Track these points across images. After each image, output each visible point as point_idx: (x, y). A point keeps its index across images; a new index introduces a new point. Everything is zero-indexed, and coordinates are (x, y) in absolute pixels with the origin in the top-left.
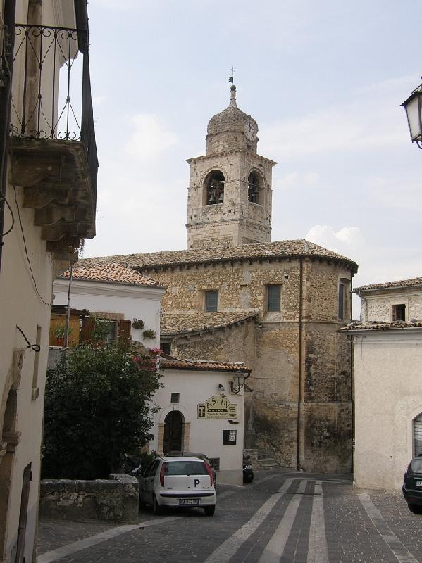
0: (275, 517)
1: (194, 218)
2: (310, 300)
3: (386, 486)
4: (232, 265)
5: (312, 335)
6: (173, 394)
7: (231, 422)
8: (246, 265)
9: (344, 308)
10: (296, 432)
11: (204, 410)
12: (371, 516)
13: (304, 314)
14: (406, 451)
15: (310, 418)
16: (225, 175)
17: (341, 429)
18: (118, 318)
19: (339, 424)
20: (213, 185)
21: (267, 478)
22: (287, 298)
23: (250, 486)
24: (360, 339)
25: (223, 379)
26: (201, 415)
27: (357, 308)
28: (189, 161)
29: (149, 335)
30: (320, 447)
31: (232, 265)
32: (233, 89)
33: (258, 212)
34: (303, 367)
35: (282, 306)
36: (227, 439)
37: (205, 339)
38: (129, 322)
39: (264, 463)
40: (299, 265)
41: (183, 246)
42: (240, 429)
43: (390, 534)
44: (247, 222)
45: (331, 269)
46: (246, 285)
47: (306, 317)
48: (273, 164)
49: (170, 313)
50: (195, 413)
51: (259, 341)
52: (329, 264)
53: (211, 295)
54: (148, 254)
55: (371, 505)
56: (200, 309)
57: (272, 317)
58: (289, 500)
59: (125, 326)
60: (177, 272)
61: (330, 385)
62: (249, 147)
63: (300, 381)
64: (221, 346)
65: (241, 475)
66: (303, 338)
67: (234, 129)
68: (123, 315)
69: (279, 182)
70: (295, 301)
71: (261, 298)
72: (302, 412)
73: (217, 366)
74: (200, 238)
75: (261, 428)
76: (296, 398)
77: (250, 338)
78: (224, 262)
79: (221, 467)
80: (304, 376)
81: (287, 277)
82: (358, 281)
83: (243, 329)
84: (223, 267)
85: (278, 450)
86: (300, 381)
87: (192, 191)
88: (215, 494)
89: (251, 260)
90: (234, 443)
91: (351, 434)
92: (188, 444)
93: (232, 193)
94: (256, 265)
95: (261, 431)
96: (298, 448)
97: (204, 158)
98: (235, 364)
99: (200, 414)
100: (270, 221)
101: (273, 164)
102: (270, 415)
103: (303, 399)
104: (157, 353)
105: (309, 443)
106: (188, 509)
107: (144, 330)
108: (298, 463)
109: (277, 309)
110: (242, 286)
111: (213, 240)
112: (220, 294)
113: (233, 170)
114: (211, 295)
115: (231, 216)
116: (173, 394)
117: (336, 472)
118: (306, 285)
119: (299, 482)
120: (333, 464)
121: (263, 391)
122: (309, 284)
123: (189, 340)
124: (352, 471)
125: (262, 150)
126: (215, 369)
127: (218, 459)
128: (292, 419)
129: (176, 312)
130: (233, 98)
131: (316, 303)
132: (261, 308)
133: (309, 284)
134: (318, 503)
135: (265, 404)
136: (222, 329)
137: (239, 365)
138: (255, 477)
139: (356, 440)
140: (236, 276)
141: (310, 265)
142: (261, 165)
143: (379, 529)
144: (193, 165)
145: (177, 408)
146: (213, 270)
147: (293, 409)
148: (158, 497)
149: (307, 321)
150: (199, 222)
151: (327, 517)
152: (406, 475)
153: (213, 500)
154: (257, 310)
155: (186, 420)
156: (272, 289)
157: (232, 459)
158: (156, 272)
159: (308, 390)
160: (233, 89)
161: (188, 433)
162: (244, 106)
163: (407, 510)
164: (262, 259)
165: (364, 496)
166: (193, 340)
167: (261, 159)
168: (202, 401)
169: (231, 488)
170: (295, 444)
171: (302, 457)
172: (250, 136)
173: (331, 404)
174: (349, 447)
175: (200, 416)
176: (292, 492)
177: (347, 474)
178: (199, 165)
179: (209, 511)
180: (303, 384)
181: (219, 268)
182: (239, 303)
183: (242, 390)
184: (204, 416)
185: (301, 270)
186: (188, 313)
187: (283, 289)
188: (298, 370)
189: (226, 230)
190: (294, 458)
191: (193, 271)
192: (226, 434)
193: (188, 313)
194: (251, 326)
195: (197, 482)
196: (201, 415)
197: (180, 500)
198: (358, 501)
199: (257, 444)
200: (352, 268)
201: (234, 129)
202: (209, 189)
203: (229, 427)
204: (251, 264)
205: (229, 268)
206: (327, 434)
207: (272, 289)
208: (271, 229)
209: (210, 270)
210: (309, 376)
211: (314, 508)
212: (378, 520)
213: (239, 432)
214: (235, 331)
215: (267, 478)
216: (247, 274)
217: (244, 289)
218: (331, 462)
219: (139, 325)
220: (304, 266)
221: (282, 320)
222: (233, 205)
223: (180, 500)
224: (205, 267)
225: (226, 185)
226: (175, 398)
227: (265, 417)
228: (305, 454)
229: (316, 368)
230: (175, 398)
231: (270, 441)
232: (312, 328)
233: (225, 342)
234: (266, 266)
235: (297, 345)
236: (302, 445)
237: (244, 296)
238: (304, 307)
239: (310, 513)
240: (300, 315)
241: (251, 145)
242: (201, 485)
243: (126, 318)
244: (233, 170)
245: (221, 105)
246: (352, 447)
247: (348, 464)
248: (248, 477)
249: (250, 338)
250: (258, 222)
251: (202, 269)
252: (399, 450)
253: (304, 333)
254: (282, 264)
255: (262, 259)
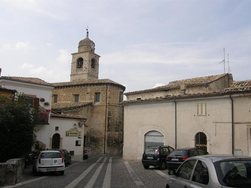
0: (94, 169)
1: (73, 73)
2: (110, 98)
3: (134, 159)
4: (84, 86)
5: (110, 110)
6: (56, 127)
7: (79, 138)
8: (89, 86)
9: (121, 99)
10: (104, 142)
11: (68, 133)
12: (130, 171)
13: (108, 102)
14: (142, 146)
15: (109, 137)
16: (84, 59)
17: (119, 140)
18: (34, 97)
19: (118, 139)
20: (79, 62)
21: (93, 157)
22: (102, 97)
23: (86, 160)
24: (126, 107)
25: (76, 122)
26: (67, 135)
27: (125, 98)
28: (72, 54)
29: (47, 104)
30: (112, 146)
31: (84, 86)
32: (88, 32)
33: (94, 71)
34: (107, 120)
35: (100, 100)
36: (77, 144)
37: (73, 110)
38: (38, 99)
39: (93, 152)
40: (106, 86)
41: (69, 81)
42: (82, 140)
43: (138, 180)
44: (90, 74)
45: (117, 88)
46: (88, 93)
47: (108, 104)
48: (100, 57)
49: (62, 102)
50: (65, 134)
51: (92, 110)
52: (116, 86)
53: (77, 96)
54: (56, 83)
55: (130, 166)
56: (73, 101)
57: (97, 104)
58: (99, 166)
59: (37, 100)
60: (65, 89)
61: (116, 126)
62: (92, 51)
63: (106, 125)
64: (79, 113)
65: (82, 156)
66: (107, 111)
67: (87, 45)
68: (36, 96)
69: (101, 61)
70: (105, 98)
71: (93, 97)
72: (106, 135)
73: (74, 117)
74: (74, 79)
75: (90, 140)
76: (104, 130)
77: (89, 111)
78: (81, 85)
79: (75, 154)
80: (107, 123)
81: (102, 90)
82: (125, 92)
83: (87, 107)
84: (81, 87)
85: (98, 147)
86: (106, 125)
87: (73, 64)
88: (64, 166)
89: (91, 85)
90: (80, 145)
91: (122, 142)
92: (62, 146)
93: (86, 65)
94: (92, 86)
95: (92, 142)
96: (105, 147)
97: (77, 53)
98: (81, 117)
99: (67, 135)
100: (98, 75)
101: (100, 57)
102: (95, 136)
103: (107, 131)
104: (49, 111)
105: (108, 145)
106: (53, 173)
107: (45, 102)
108: (104, 152)
109: (99, 101)
110: (87, 93)
111: (79, 80)
112: (79, 96)
113: (86, 57)
114: (77, 96)
115: (85, 72)
116: (56, 127)
117: (117, 154)
118: (108, 93)
119: (104, 158)
120: (116, 152)
121: (93, 128)
122: (109, 93)
123: (67, 111)
124: (122, 153)
125: (96, 52)
126: (73, 118)
127: (74, 151)
128: (103, 138)
129: (64, 102)
130: (87, 35)
131: (112, 99)
132: (94, 101)
133: (109, 93)
134: (109, 165)
135: (94, 133)
136: (79, 107)
137: (82, 117)
138: (88, 157)
139: (124, 143)
140: (85, 90)
141: (110, 86)
142: (95, 57)
143: (133, 178)
144: (74, 56)
145: (57, 132)
146: (77, 88)
147: (103, 134)
148: (37, 168)
149: (109, 105)
150: (74, 74)
151: (112, 173)
152: (143, 155)
153: (63, 169)
154: (92, 101)
155: (61, 137)
156: (97, 94)
157: (79, 151)
158: (58, 88)
159: (108, 128)
160: (88, 32)
161: (62, 142)
162: (91, 38)
163: (143, 167)
164: (94, 84)
165: (126, 163)
166: (69, 111)
167: (96, 55)
168: (68, 130)
169: (78, 162)
170: (104, 146)
171: (106, 150)
172: (92, 47)
173: (116, 132)
174: (121, 146)
175: (67, 135)
176: (101, 162)
177: (121, 154)
178: (75, 55)
179: (62, 173)
180: (107, 126)
181: (80, 87)
182: (86, 99)
183: (83, 126)
184: (68, 135)
185: (107, 88)
186: (69, 102)
187: (101, 94)
188: (105, 121)
189: (83, 76)
190: (103, 150)
191: (71, 88)
192: (77, 142)
193: (69, 102)
194: (90, 107)
195: (55, 161)
196: (67, 135)
197: (47, 169)
198: (124, 165)
199: (91, 146)
200: (124, 88)
201: (87, 45)
202: (78, 64)
203: (78, 139)
204: (90, 86)
205: (83, 87)
206: (114, 142)
207: (97, 94)
208: (98, 77)
209: (77, 88)
210: (109, 123)
211: (107, 169)
212: (132, 173)
213: (82, 141)
214: (84, 108)
215: (93, 157)
216: (89, 89)
217: (88, 94)
218: (115, 151)
219: (43, 100)
220: (108, 87)
221: (100, 105)
222: (86, 68)
223: (47, 169)
224: (75, 87)
225: (84, 62)
226: (57, 128)
227: (94, 137)
228: (107, 149)
229: (111, 121)
230: (57, 128)
231: (95, 145)
232: (110, 107)
233: (80, 112)
234: (95, 87)
235: (105, 113)
236: (106, 146)
237: (88, 96)
238: (108, 100)
239: (106, 172)
240: (106, 103)
241: (92, 51)
242: (59, 163)
243: (37, 97)
244: (86, 57)
245: (84, 37)
246: (122, 146)
247: (121, 152)
248: (85, 157)
249: (89, 111)
250: (94, 75)
251: (74, 88)
252: (139, 146)
253: (107, 109)
254: (101, 86)
255: (94, 84)
